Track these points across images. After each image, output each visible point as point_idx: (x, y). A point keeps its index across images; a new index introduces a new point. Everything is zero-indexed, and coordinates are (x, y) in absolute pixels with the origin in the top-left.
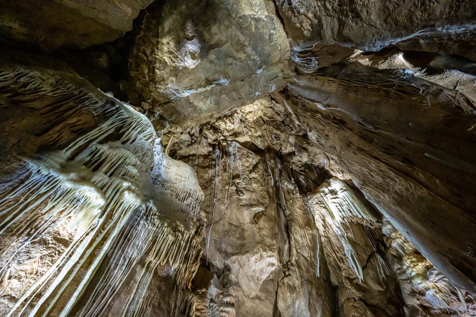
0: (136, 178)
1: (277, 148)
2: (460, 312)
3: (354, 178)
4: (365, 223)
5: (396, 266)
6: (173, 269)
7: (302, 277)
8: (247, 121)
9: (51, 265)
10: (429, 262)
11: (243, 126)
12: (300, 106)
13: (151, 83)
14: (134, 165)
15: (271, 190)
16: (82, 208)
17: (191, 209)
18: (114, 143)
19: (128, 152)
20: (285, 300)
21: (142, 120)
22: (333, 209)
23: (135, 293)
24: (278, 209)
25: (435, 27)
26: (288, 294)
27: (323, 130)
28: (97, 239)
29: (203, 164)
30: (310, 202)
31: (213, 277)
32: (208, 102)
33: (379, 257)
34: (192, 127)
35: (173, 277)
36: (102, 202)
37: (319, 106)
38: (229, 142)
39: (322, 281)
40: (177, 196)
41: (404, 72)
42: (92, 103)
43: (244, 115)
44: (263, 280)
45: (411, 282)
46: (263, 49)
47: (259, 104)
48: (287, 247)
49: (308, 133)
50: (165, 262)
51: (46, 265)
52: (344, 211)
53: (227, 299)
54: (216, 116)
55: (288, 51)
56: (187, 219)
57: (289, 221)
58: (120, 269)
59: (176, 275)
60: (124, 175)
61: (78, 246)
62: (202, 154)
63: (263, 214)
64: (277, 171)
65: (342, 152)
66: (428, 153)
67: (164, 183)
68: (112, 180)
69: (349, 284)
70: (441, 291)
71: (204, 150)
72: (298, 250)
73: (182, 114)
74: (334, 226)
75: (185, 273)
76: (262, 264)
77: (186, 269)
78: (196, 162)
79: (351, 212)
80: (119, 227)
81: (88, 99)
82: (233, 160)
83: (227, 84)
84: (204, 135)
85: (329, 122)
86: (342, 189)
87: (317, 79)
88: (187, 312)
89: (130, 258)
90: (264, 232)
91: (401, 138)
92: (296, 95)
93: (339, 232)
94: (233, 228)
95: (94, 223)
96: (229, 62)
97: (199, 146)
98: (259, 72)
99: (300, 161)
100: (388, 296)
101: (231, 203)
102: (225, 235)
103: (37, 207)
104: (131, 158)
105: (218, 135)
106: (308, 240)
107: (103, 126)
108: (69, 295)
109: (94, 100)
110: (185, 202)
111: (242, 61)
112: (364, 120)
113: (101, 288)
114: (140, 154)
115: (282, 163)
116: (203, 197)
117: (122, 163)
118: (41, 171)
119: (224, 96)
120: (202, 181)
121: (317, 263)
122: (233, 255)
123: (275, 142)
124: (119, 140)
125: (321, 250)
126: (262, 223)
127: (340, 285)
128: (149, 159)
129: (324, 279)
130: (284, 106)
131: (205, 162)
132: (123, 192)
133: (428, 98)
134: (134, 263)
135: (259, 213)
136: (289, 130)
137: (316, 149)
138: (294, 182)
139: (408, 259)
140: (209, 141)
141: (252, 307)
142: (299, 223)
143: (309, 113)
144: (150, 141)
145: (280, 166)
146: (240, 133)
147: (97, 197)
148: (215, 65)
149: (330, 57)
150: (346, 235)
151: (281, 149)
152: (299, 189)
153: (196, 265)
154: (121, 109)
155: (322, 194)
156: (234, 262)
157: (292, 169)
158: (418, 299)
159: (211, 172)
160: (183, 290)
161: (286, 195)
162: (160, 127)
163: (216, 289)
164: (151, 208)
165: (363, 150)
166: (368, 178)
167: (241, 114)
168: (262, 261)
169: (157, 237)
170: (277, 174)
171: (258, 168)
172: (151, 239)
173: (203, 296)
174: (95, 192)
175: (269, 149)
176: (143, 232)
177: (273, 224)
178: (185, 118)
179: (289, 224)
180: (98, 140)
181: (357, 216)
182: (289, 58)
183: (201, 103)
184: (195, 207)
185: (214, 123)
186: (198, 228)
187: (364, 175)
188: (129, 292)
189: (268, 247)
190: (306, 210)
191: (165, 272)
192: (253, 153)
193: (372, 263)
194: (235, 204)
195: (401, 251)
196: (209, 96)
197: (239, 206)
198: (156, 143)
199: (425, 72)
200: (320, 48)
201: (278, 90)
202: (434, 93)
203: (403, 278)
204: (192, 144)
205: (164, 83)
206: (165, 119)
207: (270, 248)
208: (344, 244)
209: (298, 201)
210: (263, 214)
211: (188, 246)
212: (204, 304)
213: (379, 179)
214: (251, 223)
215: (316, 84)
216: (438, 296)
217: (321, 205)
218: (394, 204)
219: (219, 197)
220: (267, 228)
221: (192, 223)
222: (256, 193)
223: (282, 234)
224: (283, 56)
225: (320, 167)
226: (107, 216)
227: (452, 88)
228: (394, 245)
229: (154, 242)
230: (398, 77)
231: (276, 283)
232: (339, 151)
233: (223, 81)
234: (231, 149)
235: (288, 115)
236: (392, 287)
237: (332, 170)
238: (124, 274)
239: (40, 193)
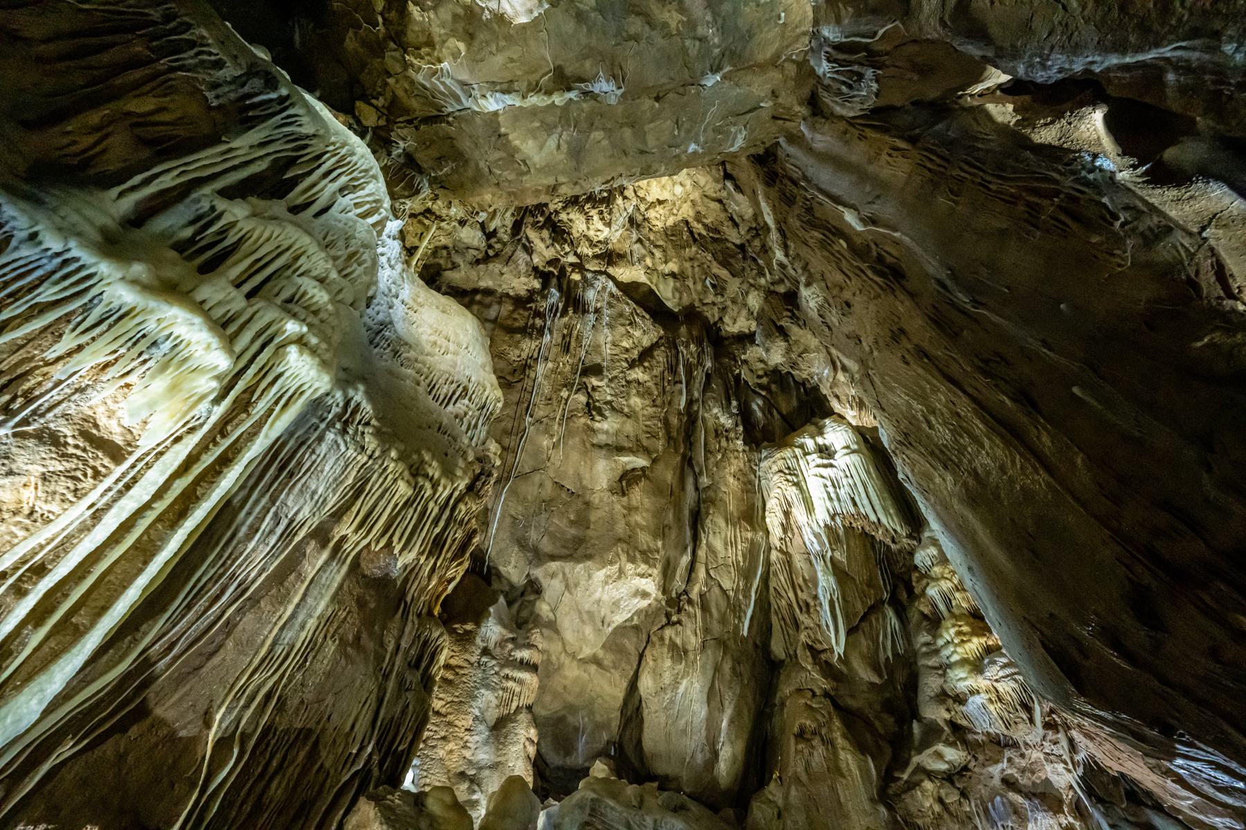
0: (323, 315)
1: (712, 314)
2: (1026, 744)
3: (886, 423)
4: (879, 535)
5: (924, 638)
6: (399, 564)
7: (706, 630)
8: (646, 224)
9: (74, 499)
10: (995, 639)
11: (635, 236)
13: (392, 45)
14: (321, 280)
15: (674, 421)
16: (164, 368)
17: (464, 428)
18: (268, 203)
19: (306, 240)
20: (657, 674)
21: (353, 154)
22: (816, 490)
23: (298, 606)
25: (1220, 40)
26: (668, 663)
27: (842, 289)
28: (204, 457)
29: (509, 322)
30: (764, 464)
31: (496, 601)
32: (552, 143)
33: (890, 613)
34: (495, 211)
35: (399, 583)
36: (222, 362)
37: (850, 218)
38: (589, 275)
39: (750, 646)
40: (431, 388)
41: (1093, 161)
42: (203, 62)
44: (614, 626)
45: (944, 675)
46: (736, 11)
47: (688, 182)
48: (685, 559)
49: (802, 288)
50: (381, 544)
51: (58, 497)
52: (839, 500)
53: (524, 654)
54: (567, 191)
55: (804, 34)
56: (450, 451)
58: (263, 541)
59: (406, 580)
60: (290, 300)
61: (148, 466)
62: (512, 293)
63: (644, 475)
64: (699, 375)
65: (876, 353)
66: (1083, 387)
67: (398, 347)
68: (255, 308)
69: (810, 660)
70: (1000, 699)
71: (519, 283)
73: (472, 164)
74: (809, 530)
75: (430, 577)
76: (621, 590)
77: (433, 570)
78: (492, 313)
79: (855, 504)
80: (266, 436)
81: (192, 44)
82: (590, 324)
83: (613, 101)
84: (524, 240)
85: (864, 266)
86: (848, 447)
87: (862, 137)
88: (423, 665)
89: (291, 521)
91: (1030, 340)
92: (796, 175)
95: (195, 412)
96: (632, 30)
97: (505, 270)
98: (709, 84)
99: (762, 361)
100: (887, 695)
101: (569, 434)
102: (540, 509)
103: (29, 340)
104: (314, 259)
105: (563, 249)
106: (740, 553)
107: (234, 145)
108: (123, 580)
109: (210, 54)
110: (450, 408)
111: (669, 35)
112: (954, 277)
113: (211, 579)
114: (343, 253)
115: (717, 357)
116: (500, 405)
117: (287, 267)
118: (40, 237)
119: (597, 135)
120: (502, 364)
121: (748, 606)
122: (553, 558)
123: (710, 298)
124: (281, 197)
126: (638, 495)
128: (365, 273)
130: (756, 204)
132: (283, 346)
133: (1130, 243)
134: (302, 534)
135: (634, 469)
136: (755, 272)
137: (809, 336)
138: (735, 411)
139: (954, 626)
140: (536, 260)
141: (578, 678)
142: (726, 511)
143: (816, 234)
144: (371, 220)
145: (709, 364)
146: (621, 256)
147: (209, 346)
148: (589, 30)
149: (916, 78)
150: (829, 554)
151: (721, 319)
154: (293, 105)
155: (798, 451)
156: (553, 576)
158: (948, 710)
159: (528, 346)
160: (419, 615)
161: (711, 440)
162: (404, 189)
164: (358, 405)
165: (927, 356)
166: (919, 429)
167: (634, 201)
168: (620, 583)
169: (368, 480)
170: (697, 381)
171: (652, 357)
172: (350, 481)
173: (465, 640)
174: (205, 329)
175: (691, 314)
176: (331, 462)
177: (663, 501)
178: (478, 180)
179: (703, 510)
180: (219, 184)
181: (866, 517)
182: (800, 59)
183: (530, 142)
184: (476, 426)
185: (557, 212)
186: (476, 478)
187: (912, 420)
188: (283, 600)
189: (643, 553)
190: (751, 483)
191: (379, 568)
192: (647, 316)
193: (871, 625)
194: (577, 439)
195: (942, 607)
196: (556, 127)
197: (588, 445)
198: (387, 231)
199: (1145, 174)
200: (896, 43)
201: (752, 151)
202: (1148, 233)
203: (930, 663)
204: (486, 259)
205: (429, 54)
206: (420, 171)
207: (647, 556)
208: (820, 575)
209: (736, 458)
210: (644, 475)
211: (445, 517)
212: (467, 656)
213: (943, 435)
214: (612, 491)
215: (857, 153)
216: (992, 708)
218: (961, 501)
219: (540, 413)
220: (647, 510)
221: (461, 463)
222: (637, 420)
223: (681, 528)
224: (787, 47)
225: (808, 386)
226: (234, 402)
227: (1195, 230)
228: (932, 592)
229: (358, 491)
230: (1074, 173)
231: (645, 637)
232: (867, 349)
233: (603, 86)
234: (591, 295)
235: (759, 230)
236: (901, 676)
237: (837, 397)
238: (272, 555)
239: (37, 300)
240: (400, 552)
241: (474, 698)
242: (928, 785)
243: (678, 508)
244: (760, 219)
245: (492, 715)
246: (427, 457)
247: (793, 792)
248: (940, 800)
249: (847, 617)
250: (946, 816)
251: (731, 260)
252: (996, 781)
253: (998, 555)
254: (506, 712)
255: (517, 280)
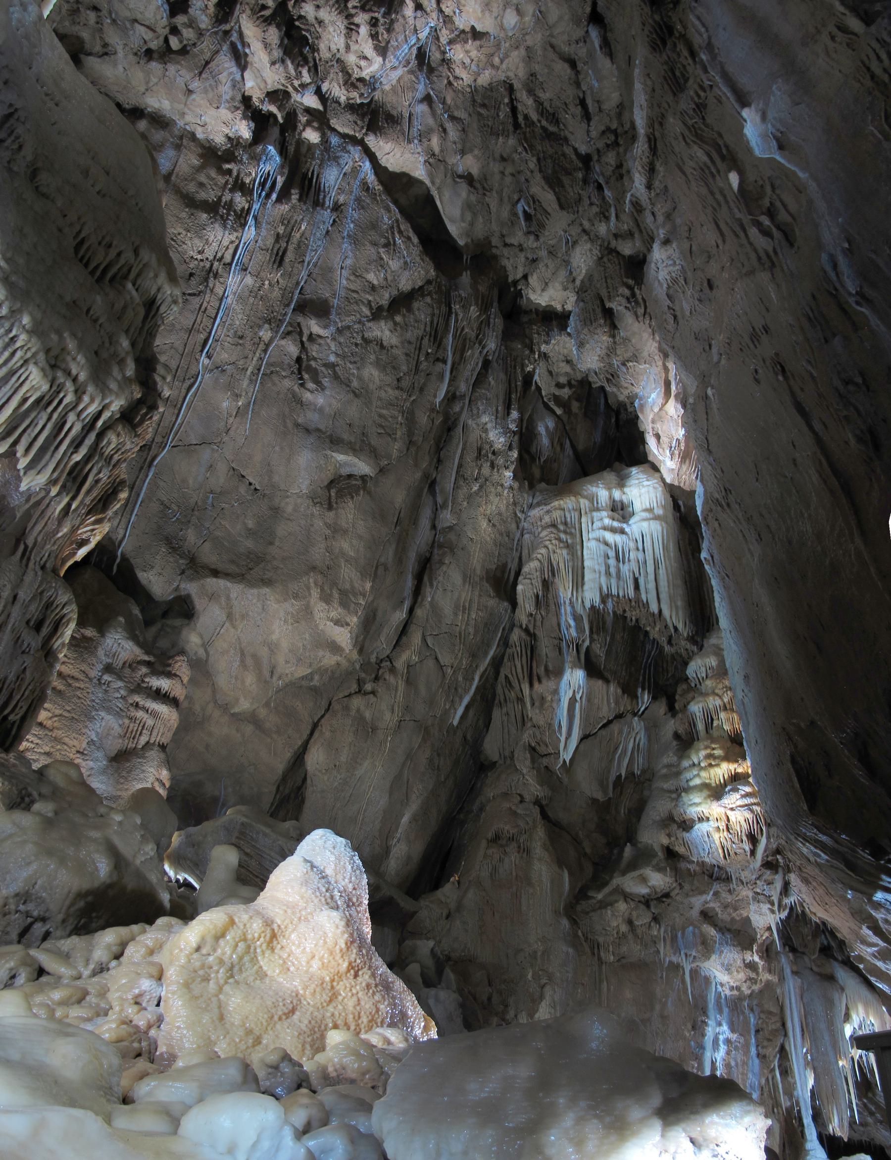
4: (655, 633)
5: (669, 758)
8: (444, 71)
11: (421, 89)
12: (685, 104)
15: (423, 419)
24: (419, 496)
29: (191, 188)
35: (18, 515)
38: (334, 140)
43: (444, 38)
48: (400, 616)
49: (656, 246)
53: (164, 684)
57: (441, 546)
59: (28, 515)
62: (200, 135)
69: (528, 763)
72: (430, 641)
74: (569, 609)
84: (234, 37)
90: (345, 545)
93: (573, 633)
94: (243, 490)
97: (195, 85)
105: (299, 75)
115: (507, 336)
121: (466, 691)
122: (215, 573)
125: (497, 664)
126: (349, 513)
127: (501, 762)
129: (465, 737)
130: (627, 83)
131: (202, 178)
135: (350, 476)
136: (595, 209)
138: (513, 427)
139: (706, 748)
140: (252, 85)
145: (492, 345)
146: (393, 120)
150: (587, 643)
151: (525, 277)
152: (521, 458)
153: (98, 522)
156: (212, 597)
157: (528, 379)
158: (669, 835)
161: (469, 458)
163: (131, 643)
167: (433, 20)
170: (469, 367)
171: (410, 310)
175: (483, 258)
179: (436, 557)
181: (647, 605)
189: (343, 593)
192: (415, 240)
195: (701, 726)
197: (290, 424)
203: (666, 786)
204: (165, 54)
209: (499, 495)
212: (84, 667)
214: (313, 498)
217: (563, 536)
220: (360, 537)
225: (623, 416)
231: (324, 704)
234: (331, 177)
235: (619, 137)
237: (658, 437)
240: (28, 468)
241: (91, 719)
242: (622, 906)
243: (402, 542)
244: (626, 116)
245: (115, 745)
246: (71, 345)
247: (470, 895)
248: (630, 922)
249: (586, 719)
250: (630, 936)
251: (566, 180)
252: (695, 913)
253: (781, 649)
254: (131, 745)
255: (212, 112)
